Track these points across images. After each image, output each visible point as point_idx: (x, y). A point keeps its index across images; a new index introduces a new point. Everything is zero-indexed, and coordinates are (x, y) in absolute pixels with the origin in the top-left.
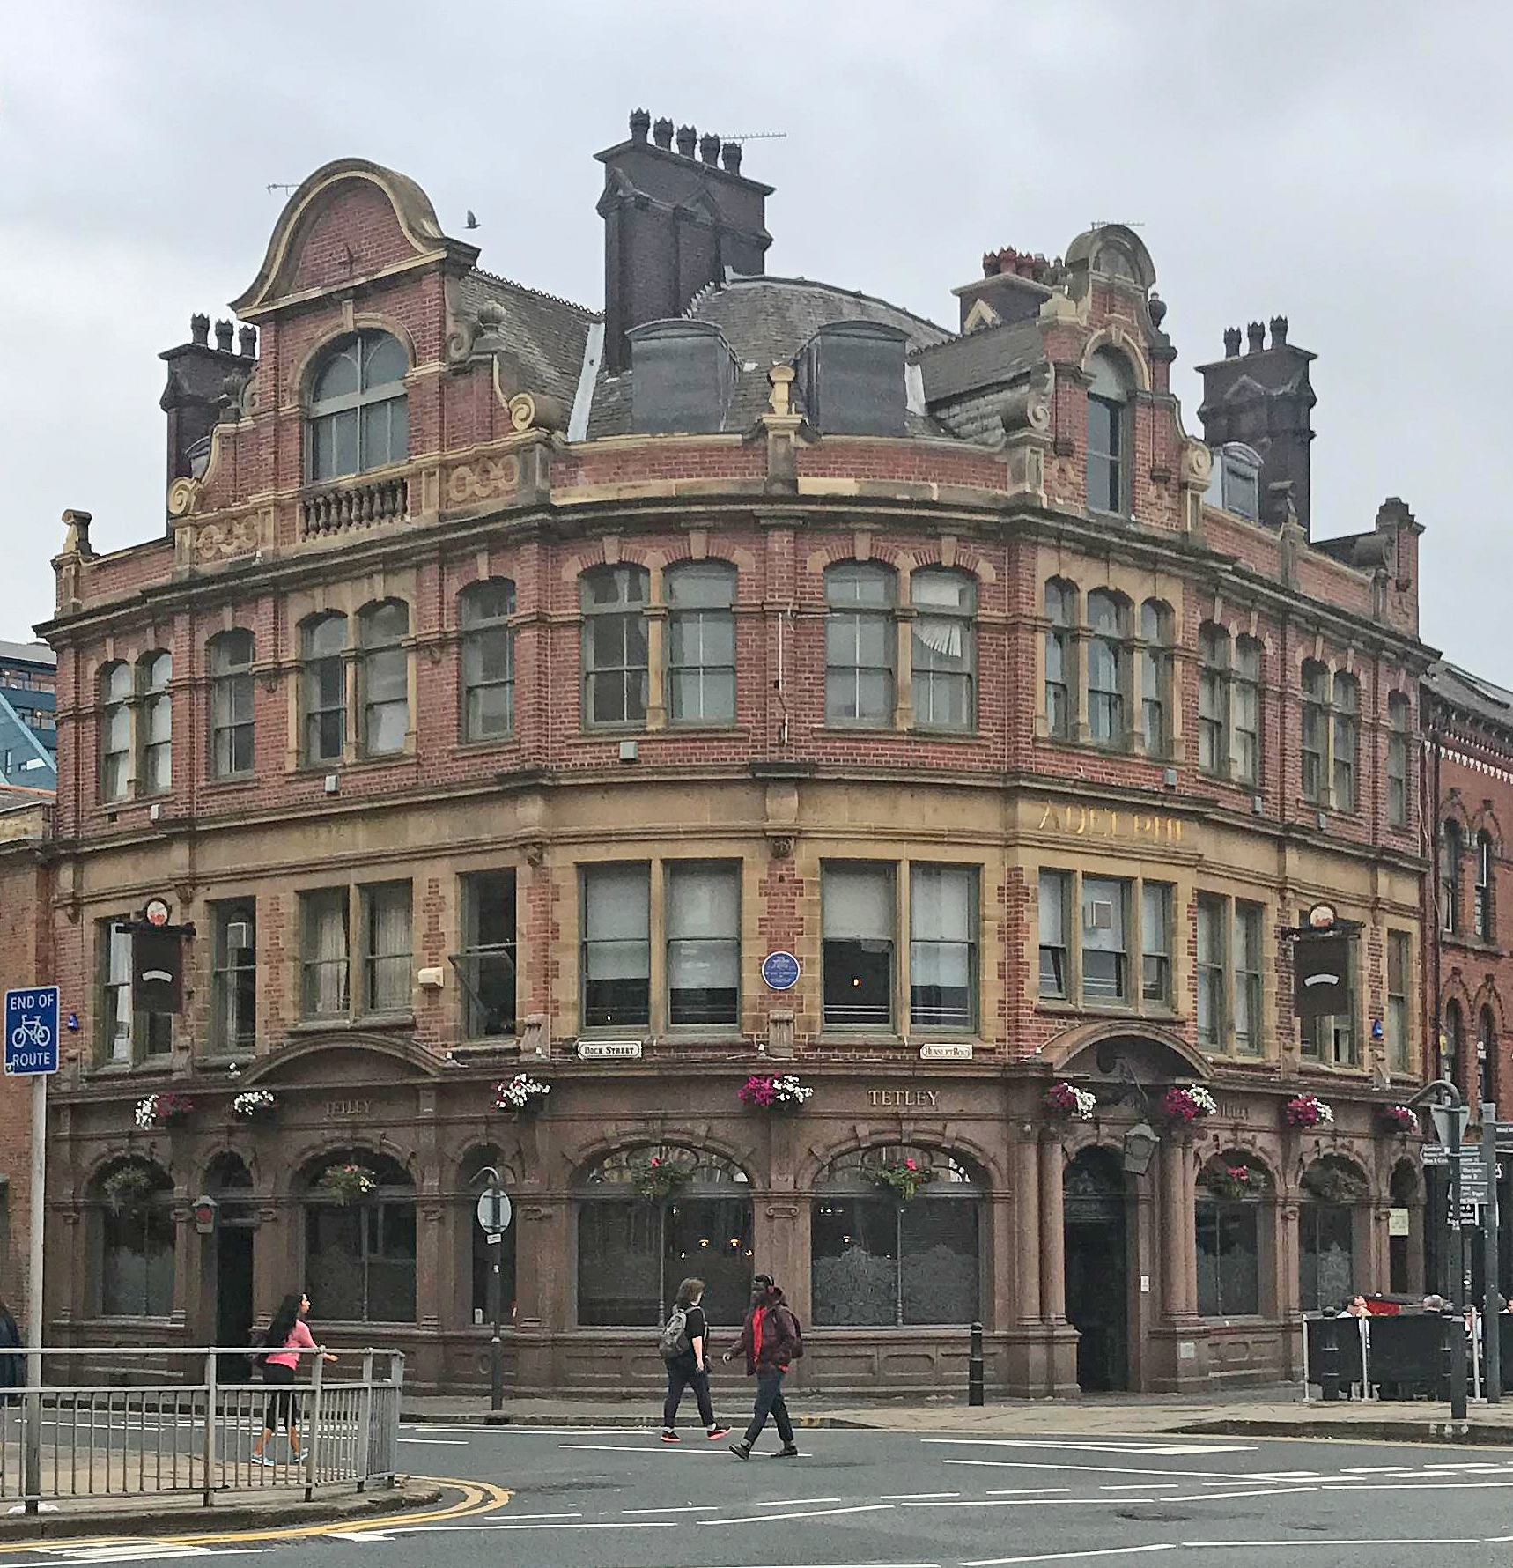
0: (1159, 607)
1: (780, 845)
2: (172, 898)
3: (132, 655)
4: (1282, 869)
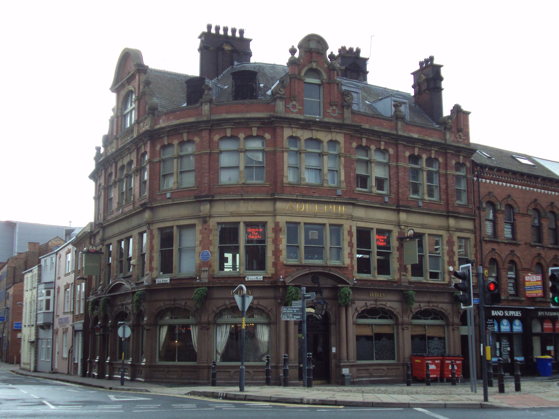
1: (205, 220)
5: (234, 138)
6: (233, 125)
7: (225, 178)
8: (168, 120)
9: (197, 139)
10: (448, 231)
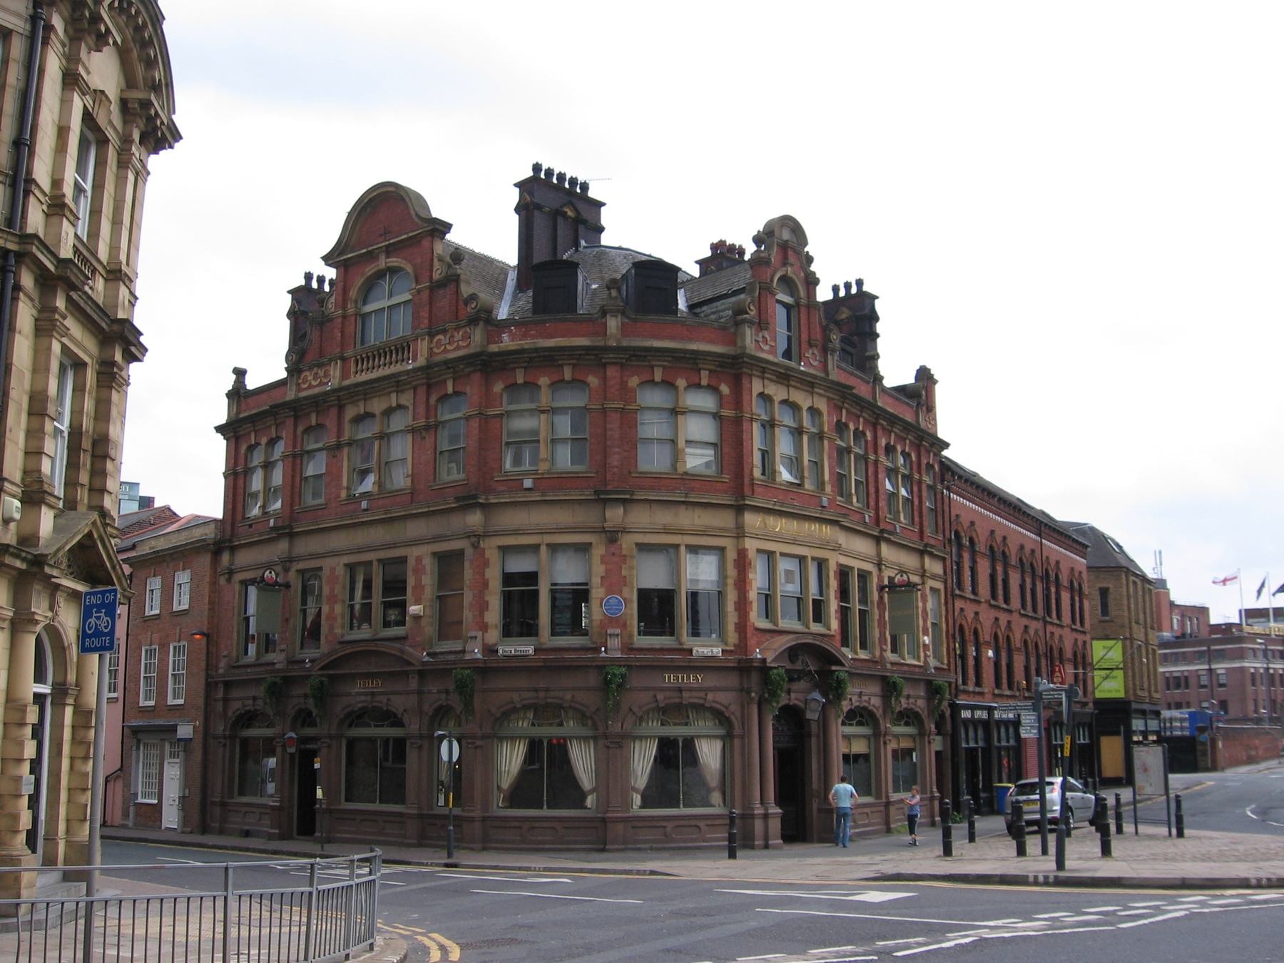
0: (813, 411)
1: (612, 536)
2: (278, 568)
3: (264, 441)
4: (879, 554)
5: (669, 384)
8: (524, 336)
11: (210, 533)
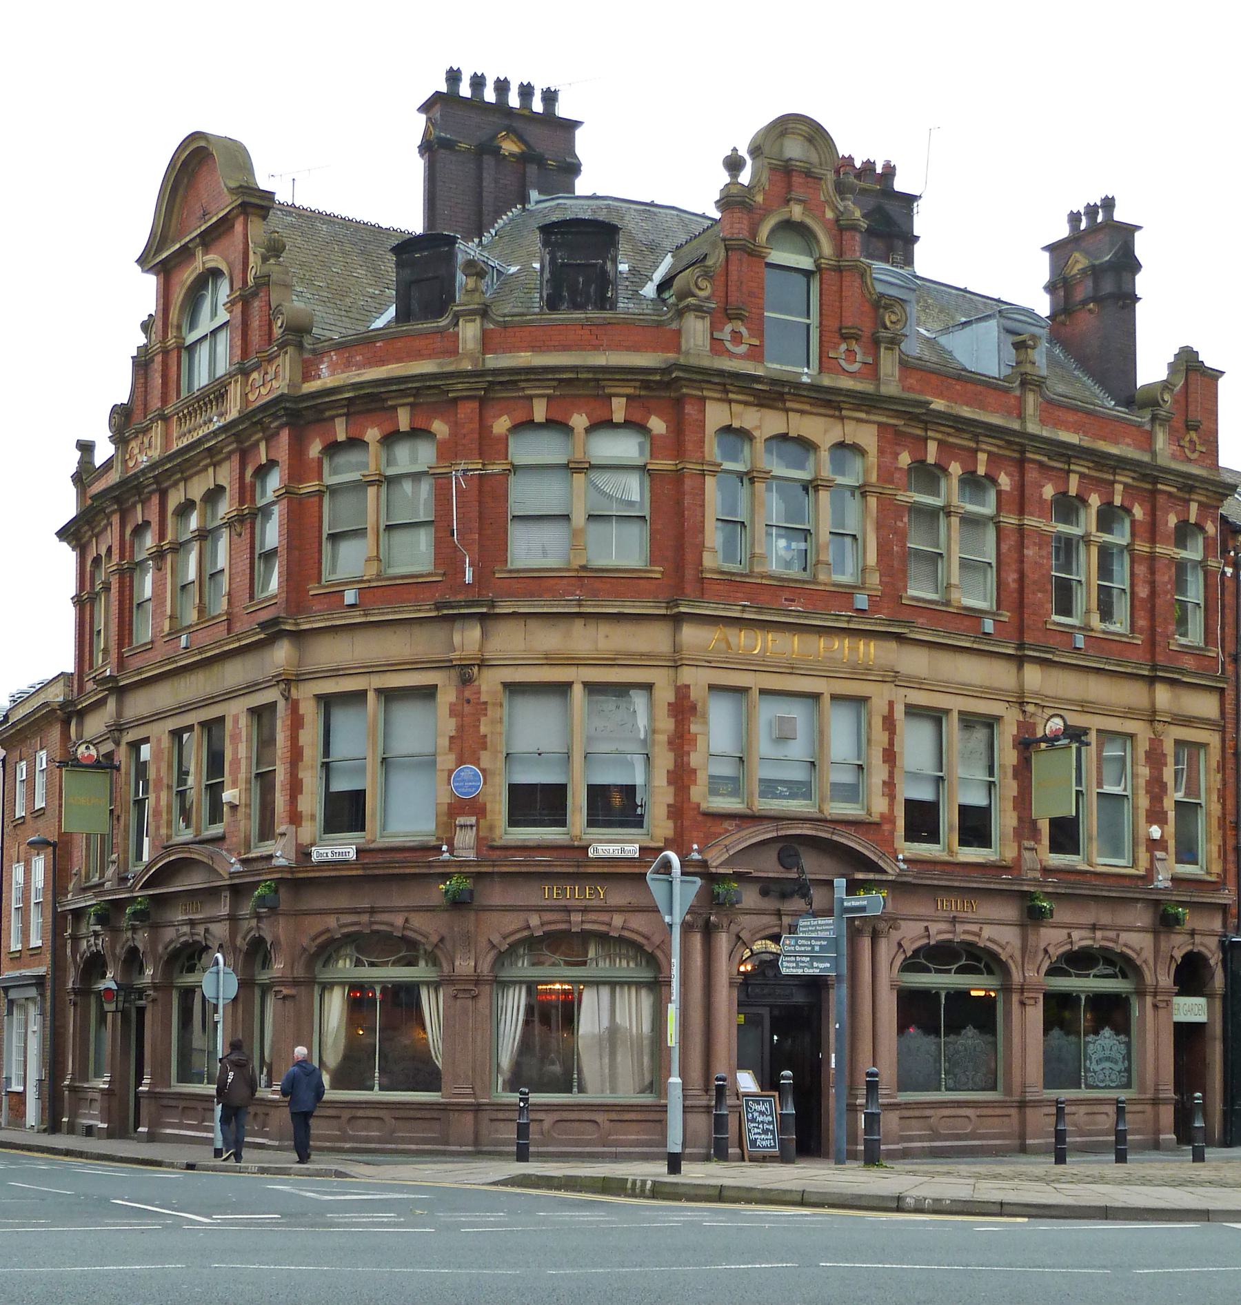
5: (556, 425)
6: (554, 388)
7: (530, 549)
8: (348, 365)
9: (440, 428)
10: (1152, 721)
11: (57, 695)
